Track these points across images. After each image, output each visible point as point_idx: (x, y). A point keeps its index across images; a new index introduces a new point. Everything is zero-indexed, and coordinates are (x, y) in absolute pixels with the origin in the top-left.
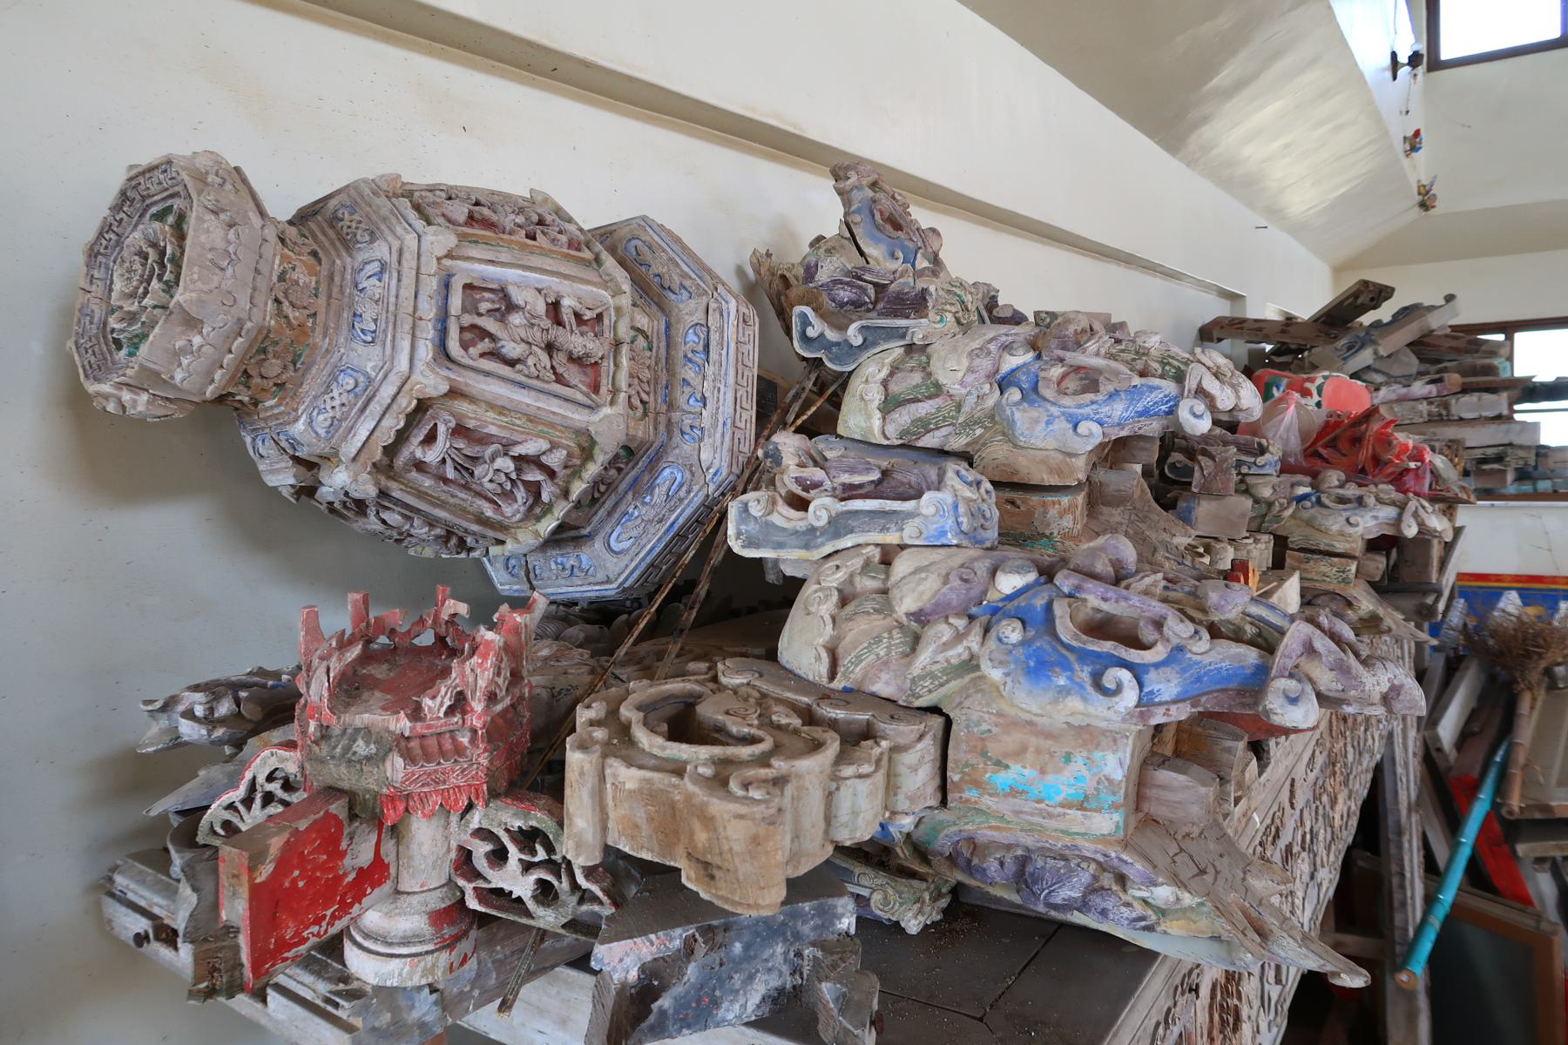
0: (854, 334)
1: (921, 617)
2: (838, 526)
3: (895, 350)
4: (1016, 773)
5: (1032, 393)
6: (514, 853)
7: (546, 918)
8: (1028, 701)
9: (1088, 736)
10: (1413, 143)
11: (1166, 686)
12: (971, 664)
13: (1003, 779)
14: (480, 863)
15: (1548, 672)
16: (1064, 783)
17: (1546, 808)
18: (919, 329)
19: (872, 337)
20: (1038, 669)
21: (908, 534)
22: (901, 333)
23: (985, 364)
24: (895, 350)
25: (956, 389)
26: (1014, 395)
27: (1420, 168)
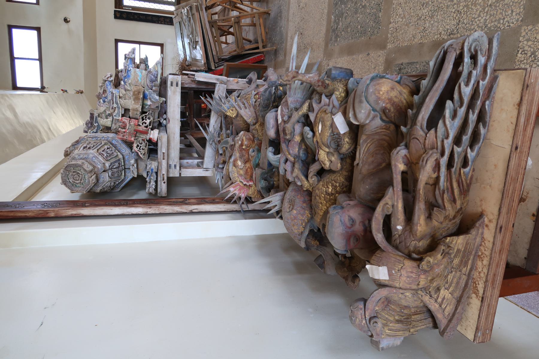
0: (96, 125)
1: (125, 90)
2: (117, 103)
3: (99, 119)
4: (139, 78)
5: (106, 97)
6: (144, 121)
7: (152, 119)
8: (132, 77)
9: (135, 72)
10: (64, 91)
11: (131, 66)
12: (130, 84)
13: (140, 80)
14: (146, 125)
15: (187, 66)
16: (139, 74)
17: (205, 64)
18: (96, 115)
19: (97, 122)
20: (129, 76)
21: (118, 95)
22: (96, 117)
23: (102, 105)
24: (99, 119)
25: (105, 108)
26: (106, 100)
27: (71, 92)
